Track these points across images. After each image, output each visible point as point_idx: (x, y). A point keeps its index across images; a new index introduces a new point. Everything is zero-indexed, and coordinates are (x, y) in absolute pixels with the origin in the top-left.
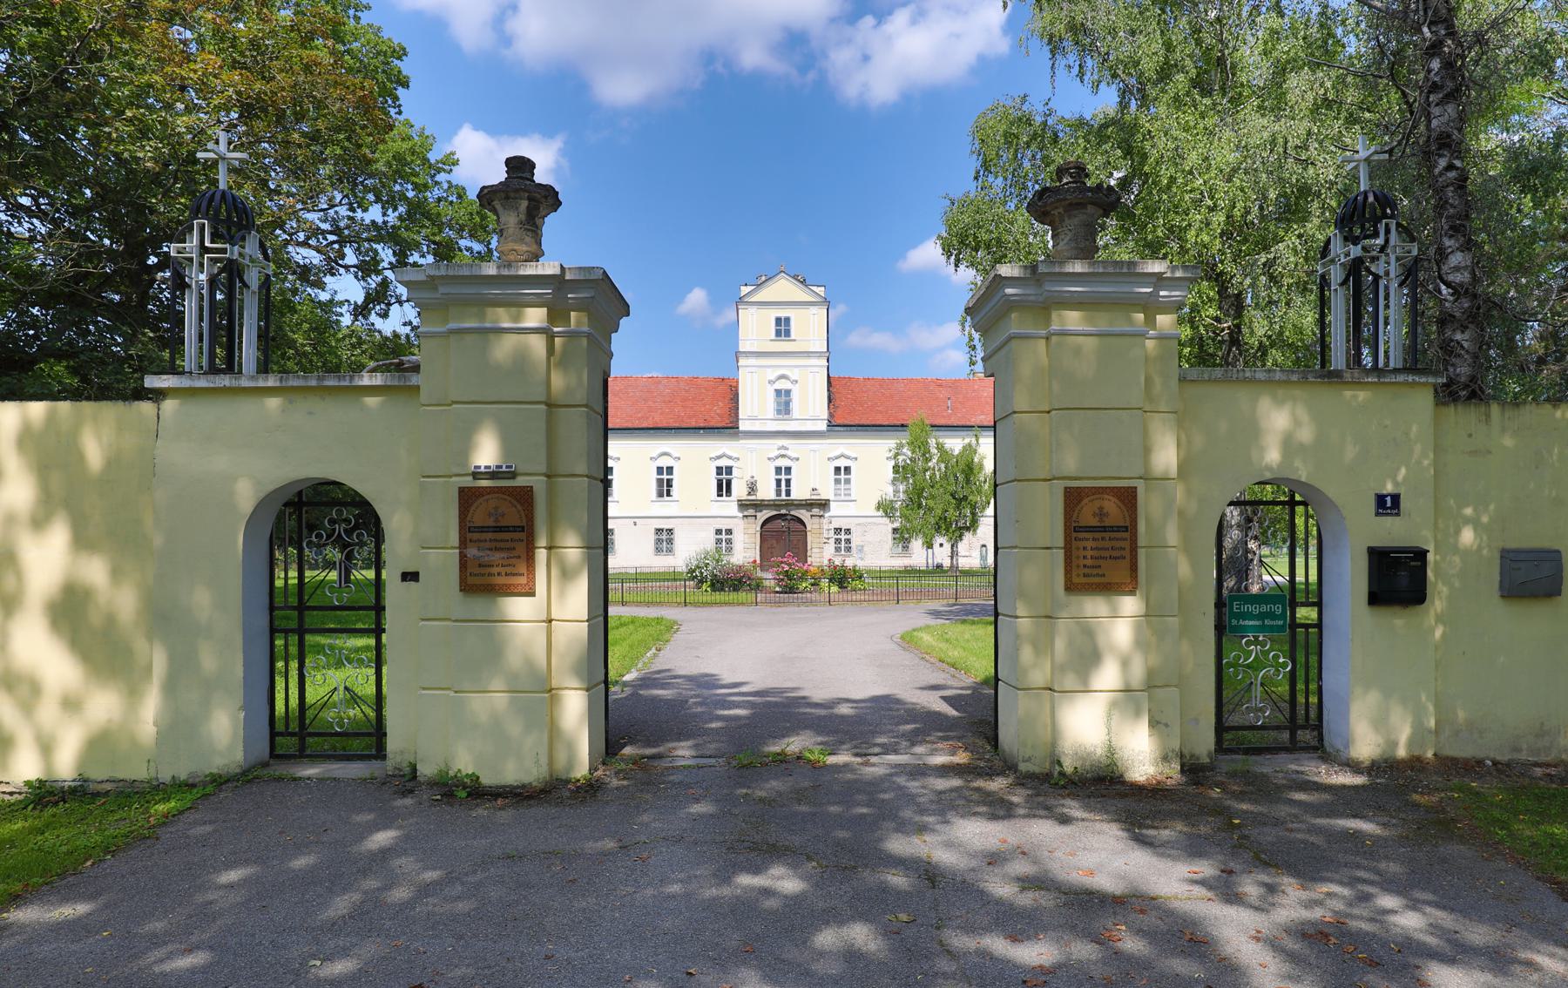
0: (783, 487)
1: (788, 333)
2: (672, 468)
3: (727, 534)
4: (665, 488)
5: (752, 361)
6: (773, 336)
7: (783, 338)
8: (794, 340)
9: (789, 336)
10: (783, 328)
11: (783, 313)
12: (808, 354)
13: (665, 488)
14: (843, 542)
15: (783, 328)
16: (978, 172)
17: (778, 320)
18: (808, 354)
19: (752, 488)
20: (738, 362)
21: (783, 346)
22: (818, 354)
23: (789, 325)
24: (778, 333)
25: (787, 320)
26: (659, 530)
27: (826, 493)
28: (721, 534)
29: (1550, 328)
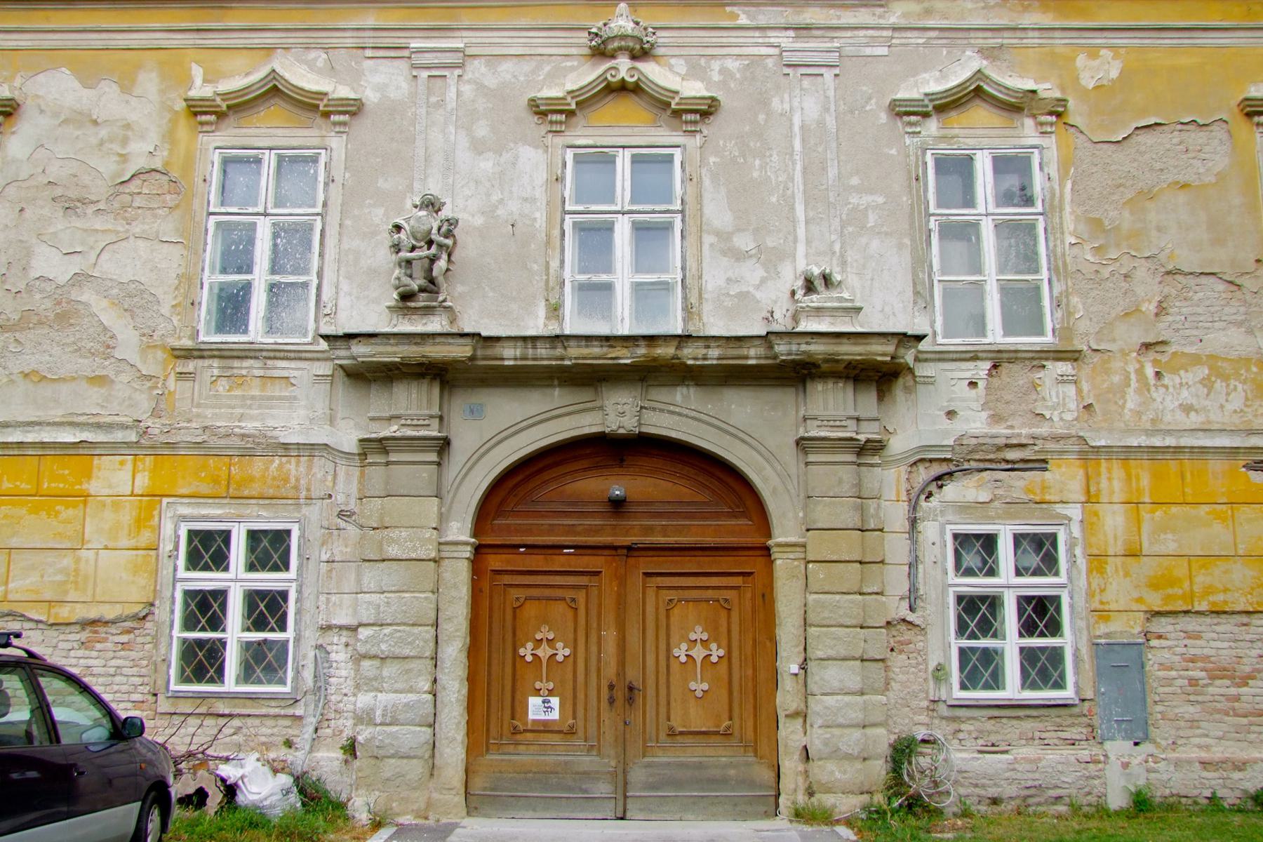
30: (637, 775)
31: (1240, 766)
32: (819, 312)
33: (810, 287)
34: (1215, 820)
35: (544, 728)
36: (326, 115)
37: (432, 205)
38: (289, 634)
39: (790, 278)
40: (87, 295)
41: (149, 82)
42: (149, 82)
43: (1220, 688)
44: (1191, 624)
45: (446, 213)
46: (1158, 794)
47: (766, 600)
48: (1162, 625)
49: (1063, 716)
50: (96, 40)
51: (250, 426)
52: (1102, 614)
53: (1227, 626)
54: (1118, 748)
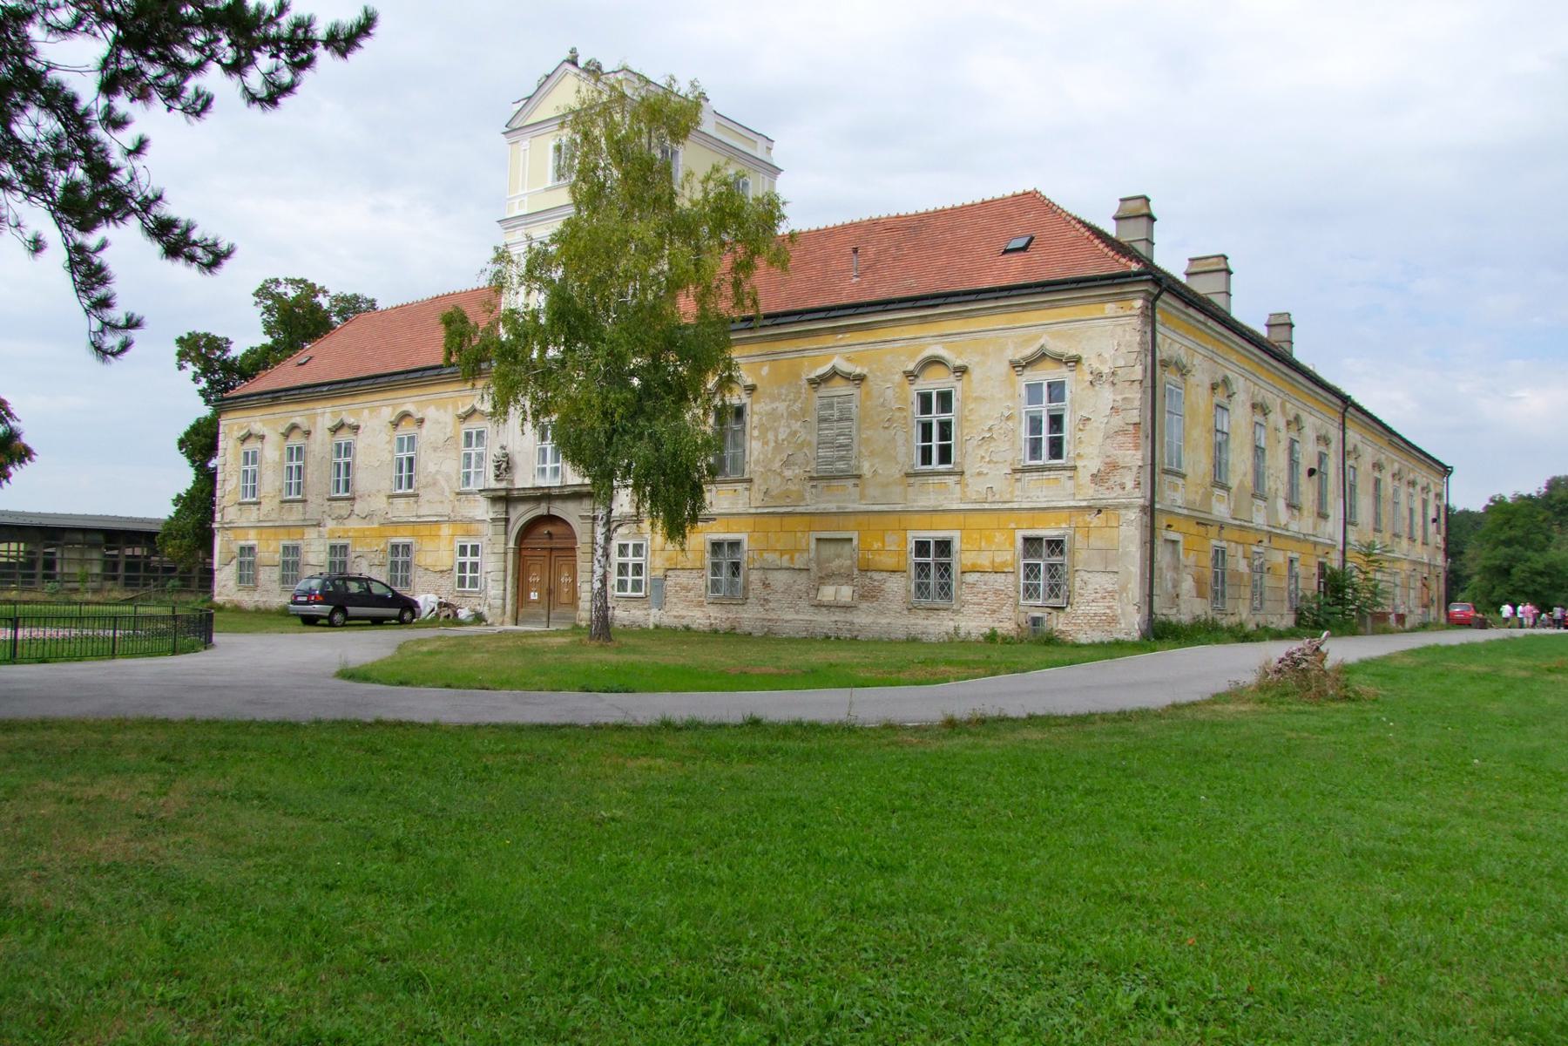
30: (552, 615)
31: (684, 617)
34: (48, 634)
35: (534, 601)
36: (1066, 363)
37: (503, 448)
38: (1022, 563)
39: (490, 471)
40: (438, 477)
41: (450, 408)
42: (450, 408)
43: (683, 593)
44: (678, 572)
46: (694, 626)
47: (574, 566)
48: (670, 573)
49: (641, 601)
50: (438, 396)
51: (471, 515)
52: (653, 569)
53: (687, 573)
54: (654, 611)
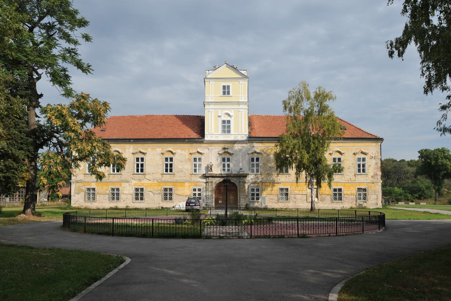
0: (361, 168)
1: (229, 93)
2: (258, 158)
3: (339, 191)
4: (169, 168)
5: (212, 106)
6: (221, 94)
7: (226, 95)
8: (231, 96)
9: (229, 94)
10: (226, 90)
11: (226, 84)
12: (238, 103)
13: (169, 168)
14: (139, 195)
15: (226, 90)
16: (405, 7)
17: (224, 87)
18: (238, 103)
19: (209, 168)
20: (205, 107)
21: (226, 99)
22: (209, 103)
23: (229, 89)
24: (224, 93)
25: (228, 87)
26: (165, 189)
27: (246, 170)
28: (196, 191)
29: (433, 67)
32: (241, 172)
33: (241, 169)
45: (212, 164)
